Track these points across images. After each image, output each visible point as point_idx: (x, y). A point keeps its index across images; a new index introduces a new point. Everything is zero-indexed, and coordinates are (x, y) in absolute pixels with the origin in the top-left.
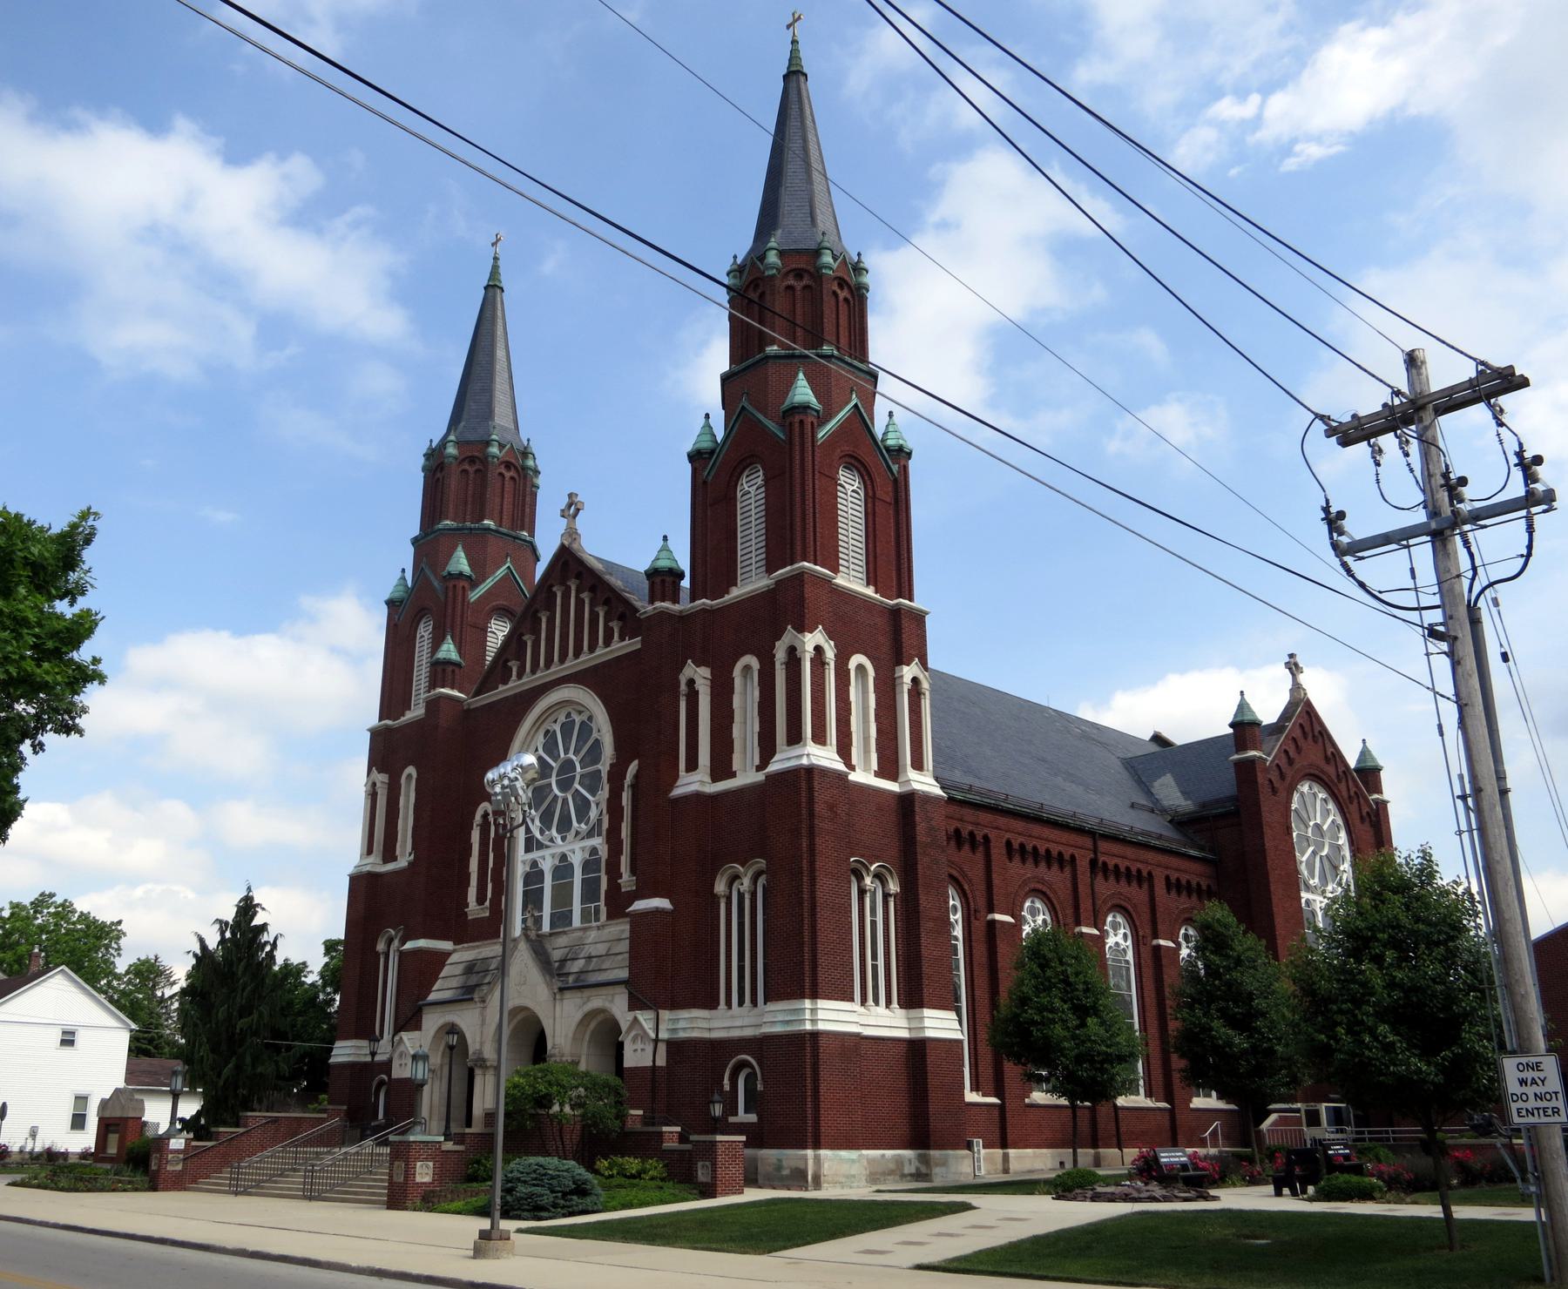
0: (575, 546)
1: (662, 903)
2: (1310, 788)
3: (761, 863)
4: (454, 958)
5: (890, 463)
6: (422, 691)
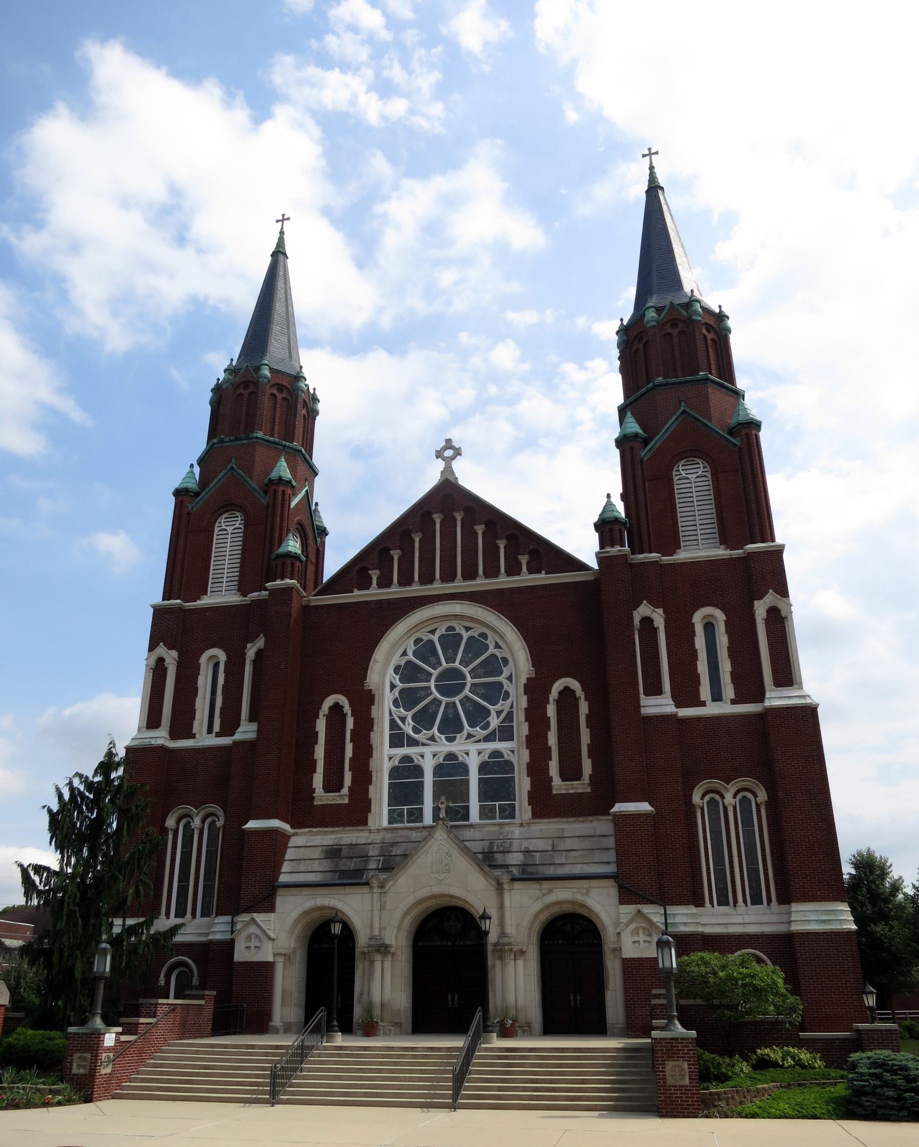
1: (645, 807)
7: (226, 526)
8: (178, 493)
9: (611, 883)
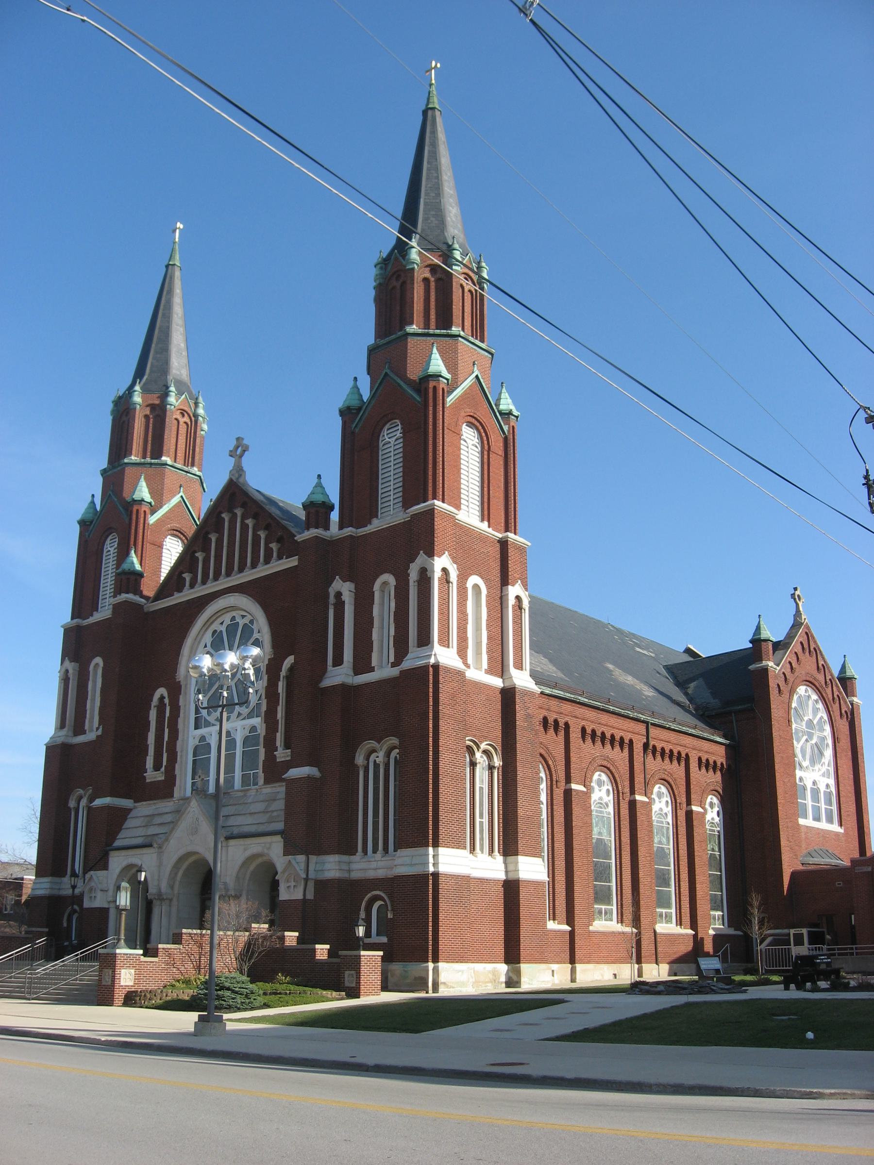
0: (241, 480)
2: (806, 691)
3: (394, 741)
4: (132, 814)
5: (502, 424)
6: (107, 596)
7: (389, 438)
8: (342, 413)
9: (278, 838)
